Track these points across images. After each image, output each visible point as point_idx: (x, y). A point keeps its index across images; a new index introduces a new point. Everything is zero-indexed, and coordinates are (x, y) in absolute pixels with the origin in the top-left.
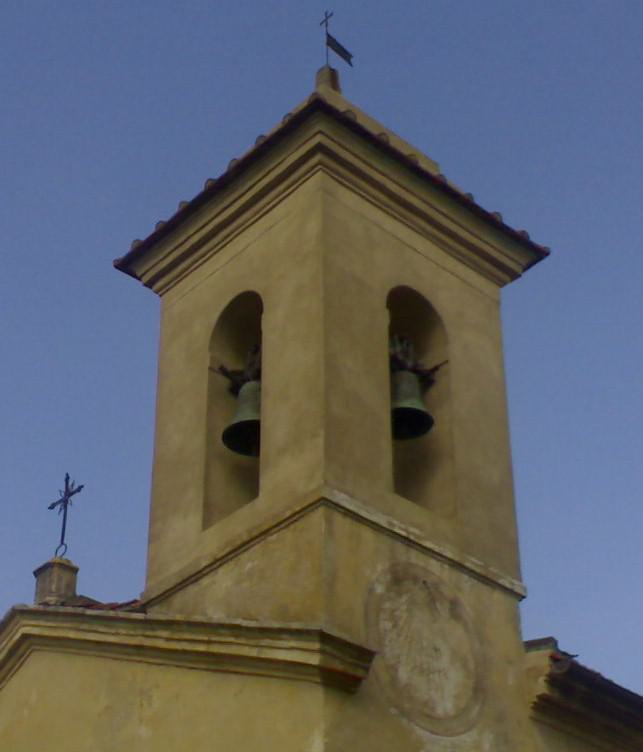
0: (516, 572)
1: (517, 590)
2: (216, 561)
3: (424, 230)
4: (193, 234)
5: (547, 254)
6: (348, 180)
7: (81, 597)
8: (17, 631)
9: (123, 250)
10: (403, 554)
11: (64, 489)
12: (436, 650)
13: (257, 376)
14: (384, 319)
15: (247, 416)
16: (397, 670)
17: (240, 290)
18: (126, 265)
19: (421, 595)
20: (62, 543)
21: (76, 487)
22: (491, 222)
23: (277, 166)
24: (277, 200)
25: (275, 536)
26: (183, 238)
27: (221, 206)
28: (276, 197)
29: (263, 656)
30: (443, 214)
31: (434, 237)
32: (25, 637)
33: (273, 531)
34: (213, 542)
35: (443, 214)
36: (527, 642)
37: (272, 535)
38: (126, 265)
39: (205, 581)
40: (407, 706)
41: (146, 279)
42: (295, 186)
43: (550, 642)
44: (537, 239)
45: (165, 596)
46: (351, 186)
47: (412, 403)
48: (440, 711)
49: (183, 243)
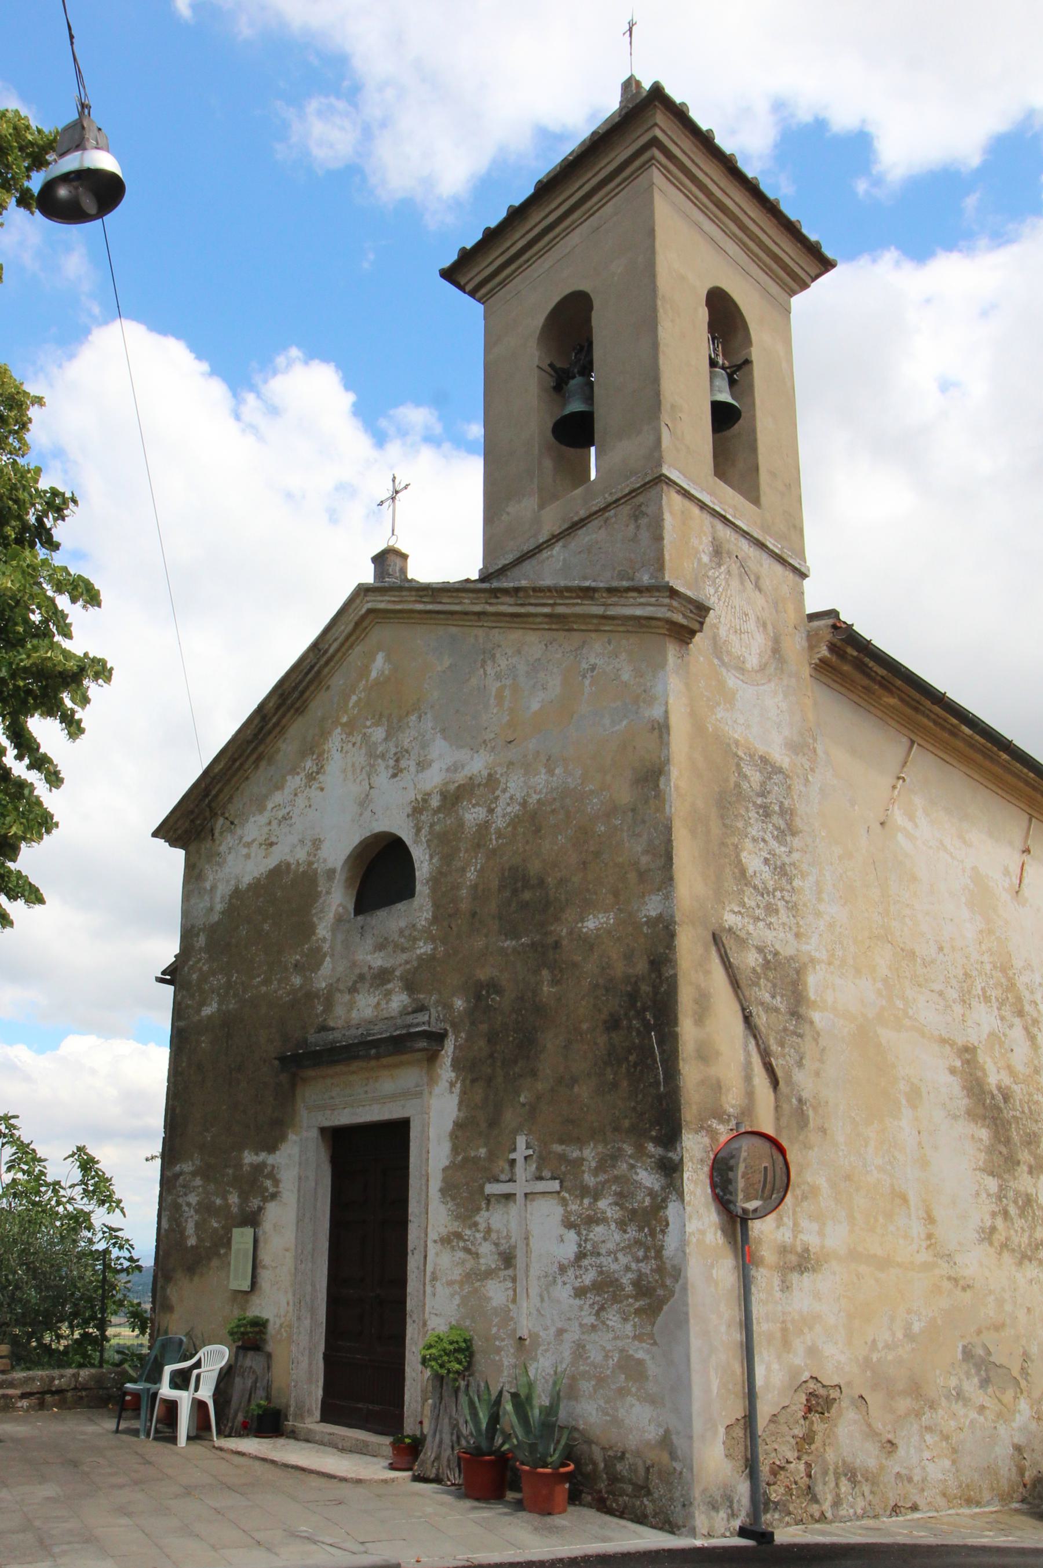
0: (801, 554)
1: (803, 569)
2: (554, 537)
3: (734, 235)
4: (517, 239)
5: (108, 679)
6: (677, 179)
7: (412, 580)
8: (362, 607)
9: (450, 258)
10: (725, 533)
11: (391, 488)
12: (746, 615)
13: (587, 368)
14: (703, 314)
15: (576, 406)
16: (718, 629)
17: (567, 291)
18: (449, 274)
19: (734, 568)
20: (393, 534)
21: (403, 485)
22: (791, 229)
23: (608, 163)
24: (608, 197)
25: (612, 511)
26: (508, 244)
27: (547, 210)
28: (606, 195)
29: (608, 613)
30: (750, 217)
31: (740, 240)
32: (370, 611)
33: (612, 507)
34: (551, 521)
35: (750, 217)
36: (808, 615)
37: (610, 510)
38: (449, 274)
39: (545, 554)
40: (726, 660)
41: (468, 288)
42: (626, 183)
43: (833, 614)
44: (828, 252)
45: (503, 571)
46: (677, 184)
47: (725, 397)
48: (748, 666)
49: (508, 248)
